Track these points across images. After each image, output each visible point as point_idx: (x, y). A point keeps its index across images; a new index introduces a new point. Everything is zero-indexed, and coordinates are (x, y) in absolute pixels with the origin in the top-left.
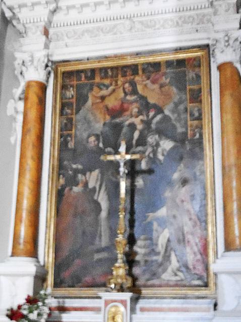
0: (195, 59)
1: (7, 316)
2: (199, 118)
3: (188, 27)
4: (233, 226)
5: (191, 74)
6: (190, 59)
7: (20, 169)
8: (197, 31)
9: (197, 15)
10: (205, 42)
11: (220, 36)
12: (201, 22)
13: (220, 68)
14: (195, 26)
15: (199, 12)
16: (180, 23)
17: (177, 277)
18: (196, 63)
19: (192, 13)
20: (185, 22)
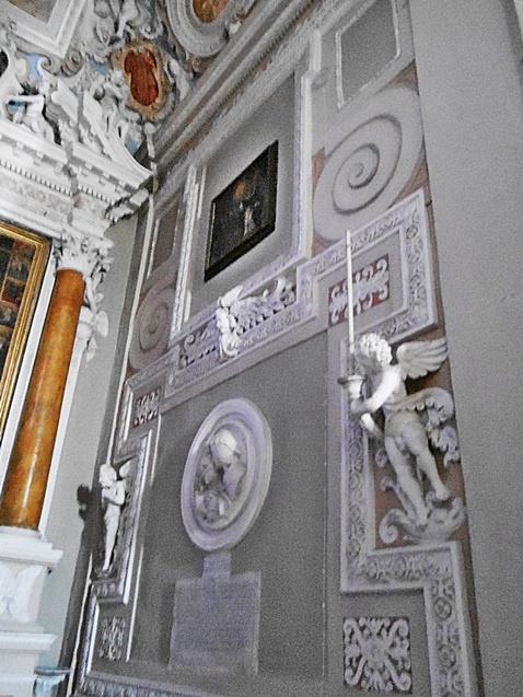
0: (28, 246)
1: (47, 19)
2: (11, 325)
3: (31, 202)
4: (25, 482)
5: (16, 263)
6: (20, 243)
7: (41, 503)
8: (45, 214)
9: (50, 195)
10: (50, 233)
11: (78, 236)
12: (53, 206)
13: (59, 275)
14: (44, 206)
15: (57, 194)
16: (25, 192)
17: (387, 665)
18: (29, 253)
19: (45, 190)
20: (31, 194)
